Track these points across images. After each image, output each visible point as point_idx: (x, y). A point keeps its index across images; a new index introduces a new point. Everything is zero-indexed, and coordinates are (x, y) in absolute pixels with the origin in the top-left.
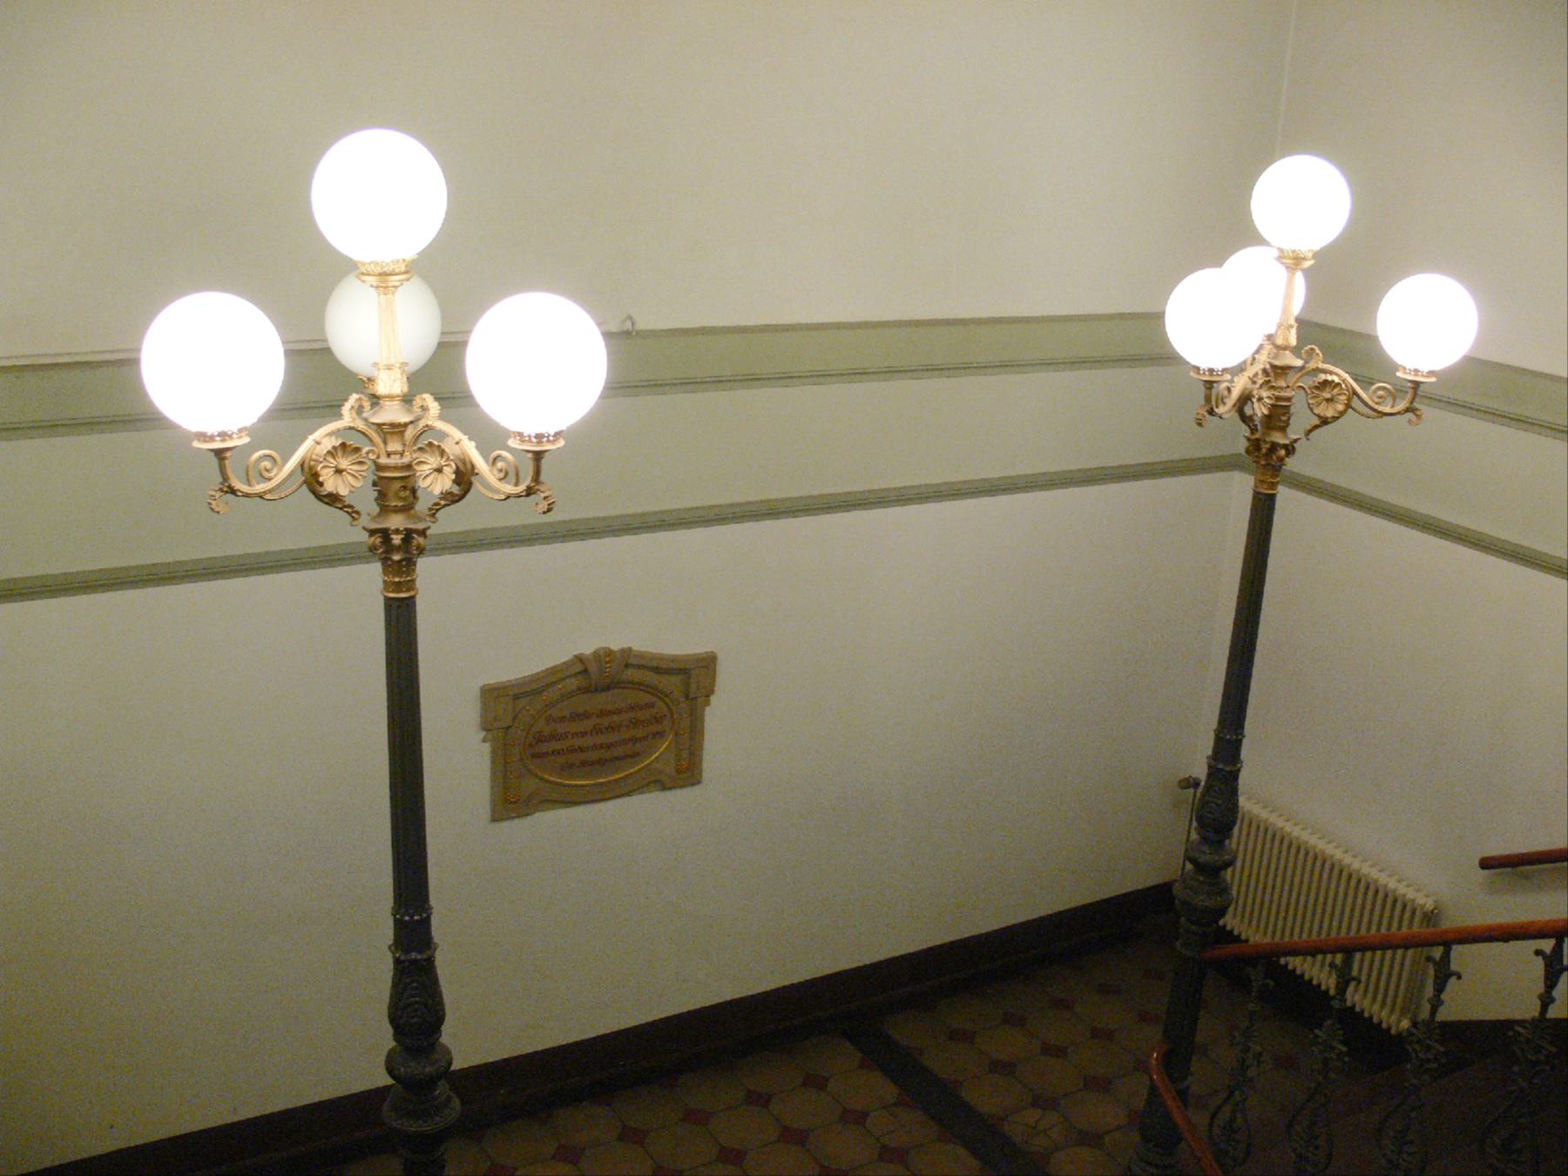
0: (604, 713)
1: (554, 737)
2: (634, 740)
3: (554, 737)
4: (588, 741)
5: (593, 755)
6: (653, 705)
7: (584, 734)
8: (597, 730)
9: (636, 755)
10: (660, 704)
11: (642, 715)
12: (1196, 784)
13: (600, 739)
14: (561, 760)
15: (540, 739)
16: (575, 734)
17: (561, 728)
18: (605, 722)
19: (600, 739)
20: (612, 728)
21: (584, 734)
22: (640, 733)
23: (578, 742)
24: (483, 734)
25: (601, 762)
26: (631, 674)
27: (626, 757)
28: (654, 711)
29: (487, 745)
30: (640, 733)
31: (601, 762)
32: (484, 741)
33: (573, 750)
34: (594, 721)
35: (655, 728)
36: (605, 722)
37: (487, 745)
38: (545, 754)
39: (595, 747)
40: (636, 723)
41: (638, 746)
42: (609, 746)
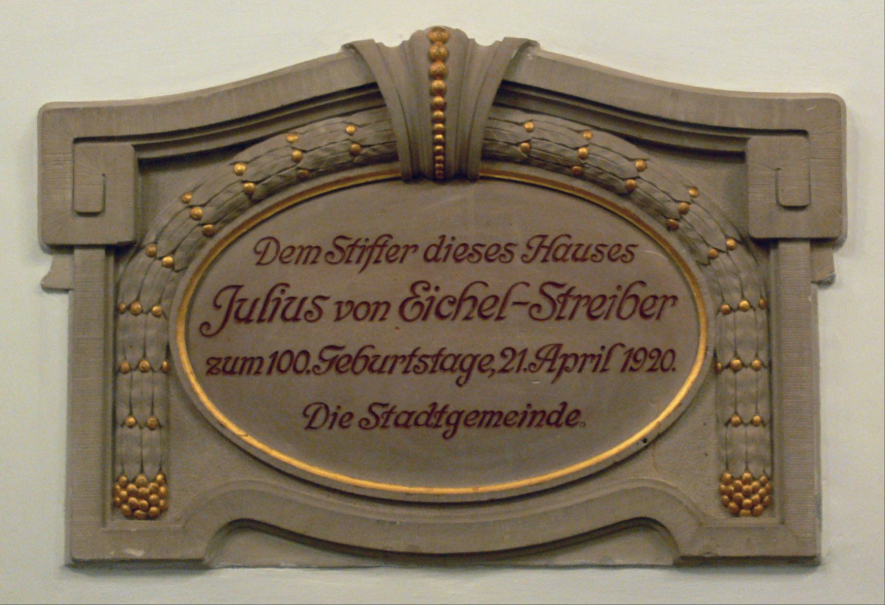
0: (442, 251)
1: (277, 306)
2: (557, 360)
3: (277, 306)
4: (392, 337)
5: (409, 392)
6: (628, 254)
7: (374, 310)
8: (424, 306)
9: (566, 417)
10: (648, 251)
11: (586, 278)
12: (749, 540)
13: (434, 336)
14: (309, 388)
15: (236, 310)
16: (350, 309)
17: (304, 281)
18: (451, 279)
19: (434, 336)
20: (485, 308)
21: (374, 310)
22: (579, 336)
23: (353, 335)
24: (44, 265)
25: (443, 420)
26: (527, 127)
27: (533, 417)
28: (626, 273)
29: (60, 304)
30: (579, 336)
31: (443, 420)
32: (48, 288)
33: (339, 362)
34: (412, 269)
35: (634, 333)
36: (451, 279)
37: (60, 304)
38: (248, 365)
39: (416, 363)
40: (560, 302)
41: (573, 388)
42: (466, 367)
